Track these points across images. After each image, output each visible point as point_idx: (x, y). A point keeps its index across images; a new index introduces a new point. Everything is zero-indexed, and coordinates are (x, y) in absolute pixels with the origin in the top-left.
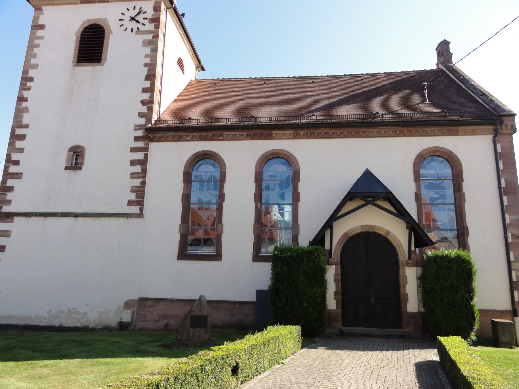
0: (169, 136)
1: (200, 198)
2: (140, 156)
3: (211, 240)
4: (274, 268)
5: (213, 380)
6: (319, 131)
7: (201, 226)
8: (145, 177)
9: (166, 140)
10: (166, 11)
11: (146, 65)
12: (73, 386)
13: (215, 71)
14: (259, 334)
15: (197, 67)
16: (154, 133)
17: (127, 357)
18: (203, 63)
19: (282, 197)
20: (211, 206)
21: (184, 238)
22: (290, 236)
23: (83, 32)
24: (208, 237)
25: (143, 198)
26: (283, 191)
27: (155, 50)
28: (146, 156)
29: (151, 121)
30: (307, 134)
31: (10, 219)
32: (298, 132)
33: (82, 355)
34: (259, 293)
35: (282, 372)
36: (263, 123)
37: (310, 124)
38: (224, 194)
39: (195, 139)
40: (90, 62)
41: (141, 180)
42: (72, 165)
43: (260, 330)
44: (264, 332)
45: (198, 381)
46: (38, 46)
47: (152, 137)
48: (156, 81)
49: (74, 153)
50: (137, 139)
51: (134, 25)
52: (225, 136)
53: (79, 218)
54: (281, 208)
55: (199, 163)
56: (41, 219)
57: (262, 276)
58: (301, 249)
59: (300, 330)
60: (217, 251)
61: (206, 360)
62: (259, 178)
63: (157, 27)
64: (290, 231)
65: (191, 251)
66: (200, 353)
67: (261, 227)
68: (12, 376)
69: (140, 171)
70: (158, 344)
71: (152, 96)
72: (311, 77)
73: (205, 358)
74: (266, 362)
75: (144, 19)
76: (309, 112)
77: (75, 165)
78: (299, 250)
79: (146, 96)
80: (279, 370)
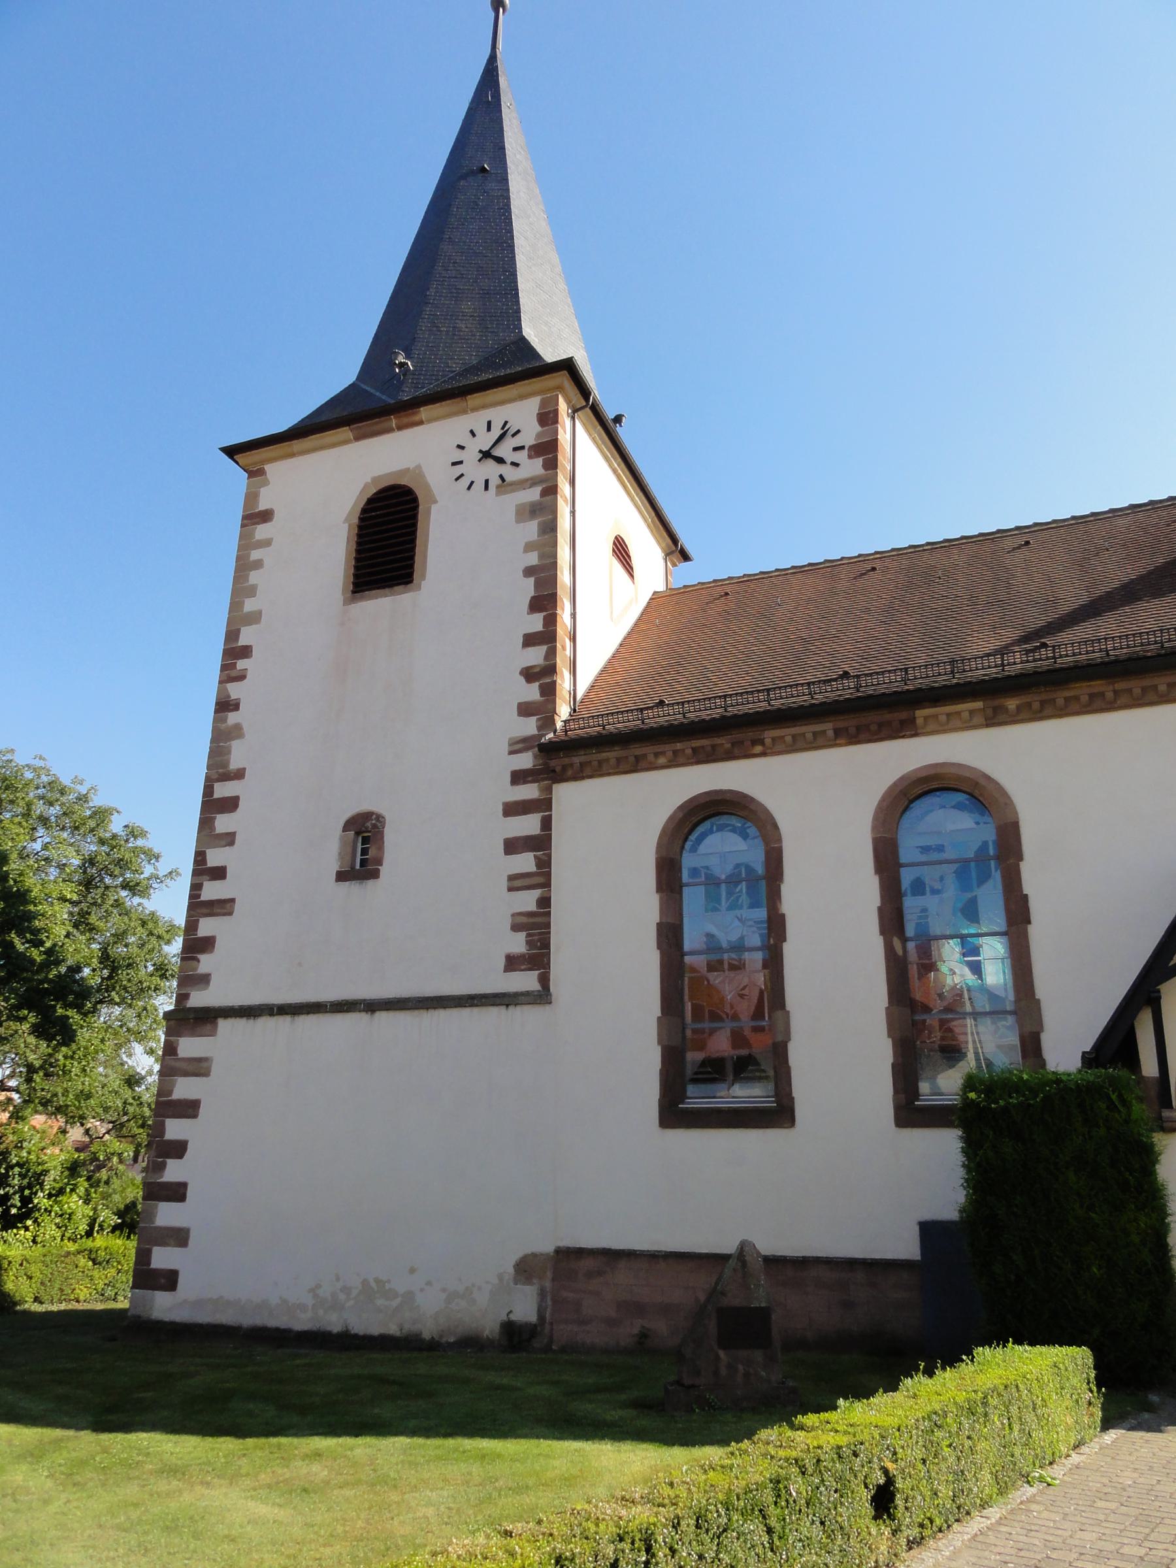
0: (607, 760)
1: (710, 936)
2: (529, 825)
3: (756, 1063)
4: (971, 1147)
5: (816, 1531)
6: (1067, 694)
7: (721, 1019)
8: (547, 884)
9: (599, 771)
10: (573, 418)
11: (529, 571)
12: (396, 1522)
13: (718, 560)
14: (949, 1373)
15: (667, 555)
16: (564, 756)
17: (538, 1437)
18: (685, 540)
19: (971, 912)
20: (747, 956)
21: (672, 1058)
22: (1014, 1039)
23: (364, 511)
24: (744, 1052)
25: (546, 945)
26: (969, 895)
27: (550, 528)
28: (547, 824)
29: (554, 724)
30: (1029, 705)
31: (209, 1027)
32: (997, 702)
33: (412, 1423)
34: (929, 1231)
35: (1045, 1514)
36: (882, 689)
37: (1036, 673)
38: (783, 915)
39: (681, 760)
40: (384, 587)
41: (536, 893)
42: (353, 867)
43: (951, 1360)
44: (966, 1367)
45: (770, 1531)
46: (258, 564)
47: (558, 769)
48: (559, 611)
49: (357, 834)
50: (518, 777)
51: (491, 470)
52: (768, 741)
53: (378, 1014)
54: (971, 951)
55: (700, 829)
56: (284, 1021)
57: (930, 1176)
58: (1058, 1081)
59: (1090, 1361)
60: (776, 1095)
61: (787, 1460)
62: (887, 859)
63: (552, 464)
64: (1010, 1020)
65: (697, 1098)
66: (764, 1434)
67: (913, 1012)
68: (233, 1479)
69: (533, 868)
70: (623, 1397)
71: (552, 653)
72: (1017, 528)
73: (782, 1453)
74: (986, 1476)
75: (515, 449)
76: (1025, 639)
77: (362, 865)
78: (1049, 1083)
79: (536, 656)
80: (1033, 1507)
